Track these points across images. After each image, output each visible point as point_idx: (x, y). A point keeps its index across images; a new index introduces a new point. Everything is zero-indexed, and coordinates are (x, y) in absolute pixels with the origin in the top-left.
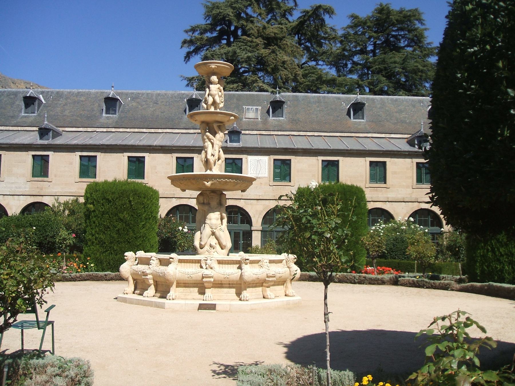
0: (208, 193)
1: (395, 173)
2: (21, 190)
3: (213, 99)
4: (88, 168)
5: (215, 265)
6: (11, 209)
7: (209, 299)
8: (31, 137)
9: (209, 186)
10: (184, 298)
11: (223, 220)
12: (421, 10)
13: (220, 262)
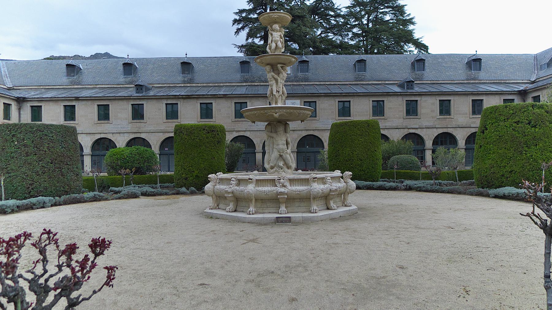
0: (275, 123)
1: (391, 108)
5: (287, 184)
6: (119, 143)
8: (132, 92)
13: (291, 181)
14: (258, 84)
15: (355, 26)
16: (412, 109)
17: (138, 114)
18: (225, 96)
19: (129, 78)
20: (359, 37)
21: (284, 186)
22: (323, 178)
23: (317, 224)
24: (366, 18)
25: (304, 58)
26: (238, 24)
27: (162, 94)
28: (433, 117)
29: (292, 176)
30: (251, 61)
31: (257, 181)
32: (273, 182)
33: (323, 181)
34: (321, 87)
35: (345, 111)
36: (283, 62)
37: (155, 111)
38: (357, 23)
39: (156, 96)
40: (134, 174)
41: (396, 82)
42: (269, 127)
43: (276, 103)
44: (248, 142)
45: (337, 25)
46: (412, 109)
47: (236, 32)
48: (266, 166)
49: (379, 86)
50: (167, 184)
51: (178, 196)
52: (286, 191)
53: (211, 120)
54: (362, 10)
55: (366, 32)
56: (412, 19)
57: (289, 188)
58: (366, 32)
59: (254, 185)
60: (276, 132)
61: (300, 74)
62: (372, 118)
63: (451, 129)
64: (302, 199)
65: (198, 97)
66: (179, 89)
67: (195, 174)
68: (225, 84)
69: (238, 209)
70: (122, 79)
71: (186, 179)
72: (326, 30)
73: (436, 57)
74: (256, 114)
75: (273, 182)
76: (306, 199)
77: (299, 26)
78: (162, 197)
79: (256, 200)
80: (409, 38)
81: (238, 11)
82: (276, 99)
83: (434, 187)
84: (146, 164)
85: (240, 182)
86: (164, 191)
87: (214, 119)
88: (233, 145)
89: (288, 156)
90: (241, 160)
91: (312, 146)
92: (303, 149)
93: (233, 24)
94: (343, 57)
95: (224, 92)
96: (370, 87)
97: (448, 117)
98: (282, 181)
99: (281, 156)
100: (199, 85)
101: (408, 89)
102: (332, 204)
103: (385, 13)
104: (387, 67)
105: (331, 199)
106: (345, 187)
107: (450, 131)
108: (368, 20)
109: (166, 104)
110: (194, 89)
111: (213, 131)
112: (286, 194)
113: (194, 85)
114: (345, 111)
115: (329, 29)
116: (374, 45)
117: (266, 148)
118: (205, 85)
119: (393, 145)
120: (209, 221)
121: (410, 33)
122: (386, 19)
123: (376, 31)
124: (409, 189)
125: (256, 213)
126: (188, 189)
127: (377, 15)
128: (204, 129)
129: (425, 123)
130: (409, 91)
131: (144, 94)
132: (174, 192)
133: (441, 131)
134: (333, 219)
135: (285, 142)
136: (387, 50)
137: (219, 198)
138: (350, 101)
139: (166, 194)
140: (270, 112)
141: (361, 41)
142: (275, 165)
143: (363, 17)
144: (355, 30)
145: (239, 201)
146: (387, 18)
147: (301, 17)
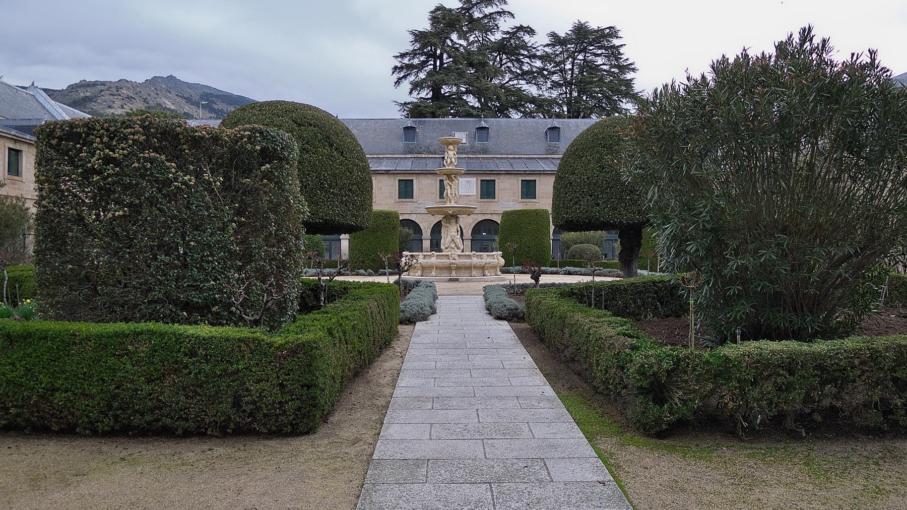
18: (387, 173)
25: (483, 124)
45: (530, 72)
48: (442, 247)
61: (477, 143)
72: (517, 77)
76: (469, 268)
92: (478, 237)
121: (629, 83)
140: (446, 210)
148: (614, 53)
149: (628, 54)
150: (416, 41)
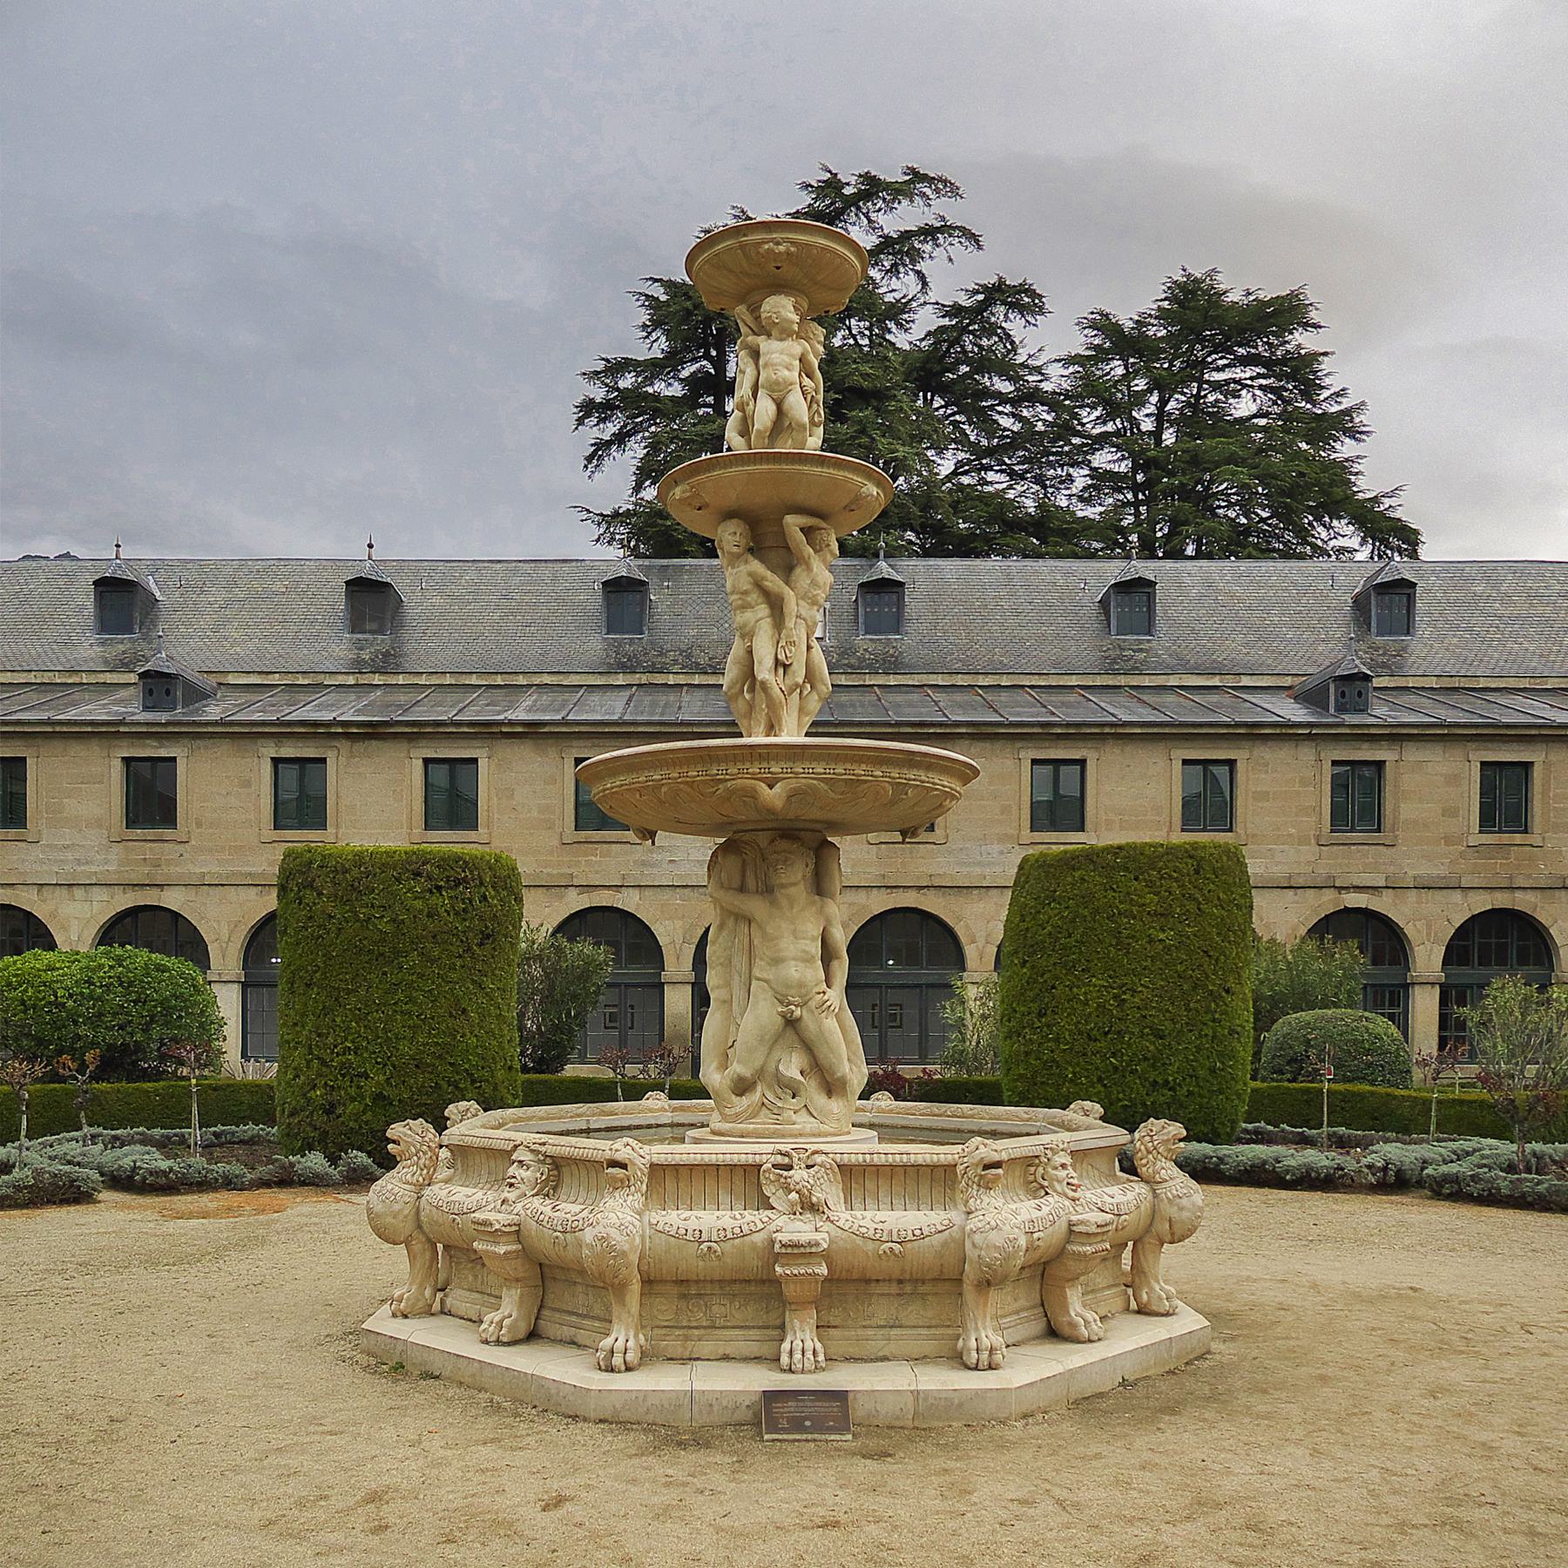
0: (763, 839)
1: (1262, 796)
2: (93, 869)
3: (779, 405)
4: (300, 801)
5: (829, 1192)
6: (65, 929)
7: (809, 1365)
8: (128, 707)
9: (779, 804)
10: (679, 1352)
11: (835, 963)
12: (1311, 296)
13: (853, 1175)
14: (681, 679)
15: (1102, 440)
16: (1358, 801)
17: (150, 801)
19: (122, 645)
20: (1120, 490)
21: (810, 1206)
22: (1030, 1161)
23: (1002, 1446)
24: (1151, 409)
25: (884, 569)
26: (602, 420)
27: (256, 717)
28: (1448, 840)
29: (863, 1147)
30: (653, 582)
31: (658, 1171)
32: (746, 1181)
33: (1030, 1175)
34: (958, 697)
35: (1059, 808)
36: (813, 502)
37: (226, 799)
38: (1110, 427)
39: (231, 724)
40: (96, 1078)
41: (1288, 681)
42: (732, 862)
43: (771, 729)
44: (625, 934)
45: (1027, 435)
46: (1358, 801)
47: (589, 459)
48: (711, 1075)
49: (1214, 698)
50: (250, 1129)
51: (282, 1196)
52: (822, 1238)
53: (471, 835)
54: (1136, 373)
55: (1148, 461)
56: (1347, 412)
57: (842, 1215)
58: (1148, 461)
59: (636, 1199)
60: (768, 891)
61: (864, 642)
62: (1179, 838)
63: (1530, 897)
64: (915, 1281)
65: (416, 733)
66: (332, 697)
67: (370, 1087)
68: (537, 680)
69: (549, 1327)
70: (89, 650)
71: (330, 1110)
72: (981, 458)
73: (1457, 571)
74: (658, 786)
75: (746, 1181)
76: (935, 1287)
77: (863, 432)
78: (207, 1200)
79: (648, 1282)
80: (1333, 494)
81: (600, 366)
82: (773, 707)
83: (1530, 1182)
84: (156, 1031)
85: (558, 1173)
86: (221, 1168)
87: (482, 833)
88: (559, 951)
89: (831, 1023)
90: (593, 1015)
91: (909, 957)
92: (873, 973)
93: (580, 421)
94: (1049, 570)
95: (529, 710)
96: (1170, 698)
97: (1518, 838)
98: (798, 1175)
99: (791, 1023)
100: (423, 680)
101: (1341, 709)
102: (1077, 1308)
103: (1231, 389)
104: (1252, 614)
105: (1073, 1279)
106: (1145, 1207)
107: (1522, 902)
108: (1160, 417)
109: (276, 761)
110: (402, 698)
111: (458, 883)
112: (826, 1256)
113: (401, 680)
114: (1059, 808)
115: (990, 452)
116: (1186, 523)
117: (712, 979)
118: (448, 680)
119: (1274, 962)
120: (374, 1393)
121: (1340, 472)
122: (1238, 414)
123: (1195, 461)
124: (1395, 1183)
125: (648, 1357)
126: (333, 1160)
127: (1198, 397)
128: (417, 874)
129: (1415, 867)
130: (1350, 719)
131: (179, 713)
132: (263, 1170)
133: (1482, 903)
134: (1089, 1405)
135: (816, 949)
136: (1237, 543)
137: (447, 1257)
138: (1082, 763)
139: (229, 1184)
140: (740, 777)
141: (1129, 504)
142: (760, 1073)
143: (1139, 400)
144: (1103, 459)
145: (557, 1291)
146: (1244, 406)
147: (874, 397)
148: (1301, 373)
149: (1346, 376)
150: (657, 324)
